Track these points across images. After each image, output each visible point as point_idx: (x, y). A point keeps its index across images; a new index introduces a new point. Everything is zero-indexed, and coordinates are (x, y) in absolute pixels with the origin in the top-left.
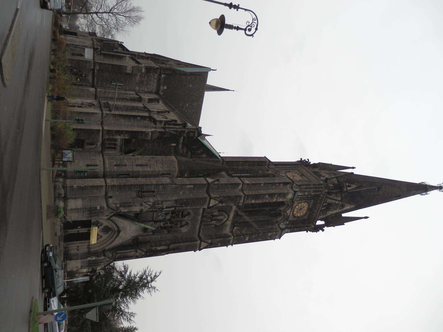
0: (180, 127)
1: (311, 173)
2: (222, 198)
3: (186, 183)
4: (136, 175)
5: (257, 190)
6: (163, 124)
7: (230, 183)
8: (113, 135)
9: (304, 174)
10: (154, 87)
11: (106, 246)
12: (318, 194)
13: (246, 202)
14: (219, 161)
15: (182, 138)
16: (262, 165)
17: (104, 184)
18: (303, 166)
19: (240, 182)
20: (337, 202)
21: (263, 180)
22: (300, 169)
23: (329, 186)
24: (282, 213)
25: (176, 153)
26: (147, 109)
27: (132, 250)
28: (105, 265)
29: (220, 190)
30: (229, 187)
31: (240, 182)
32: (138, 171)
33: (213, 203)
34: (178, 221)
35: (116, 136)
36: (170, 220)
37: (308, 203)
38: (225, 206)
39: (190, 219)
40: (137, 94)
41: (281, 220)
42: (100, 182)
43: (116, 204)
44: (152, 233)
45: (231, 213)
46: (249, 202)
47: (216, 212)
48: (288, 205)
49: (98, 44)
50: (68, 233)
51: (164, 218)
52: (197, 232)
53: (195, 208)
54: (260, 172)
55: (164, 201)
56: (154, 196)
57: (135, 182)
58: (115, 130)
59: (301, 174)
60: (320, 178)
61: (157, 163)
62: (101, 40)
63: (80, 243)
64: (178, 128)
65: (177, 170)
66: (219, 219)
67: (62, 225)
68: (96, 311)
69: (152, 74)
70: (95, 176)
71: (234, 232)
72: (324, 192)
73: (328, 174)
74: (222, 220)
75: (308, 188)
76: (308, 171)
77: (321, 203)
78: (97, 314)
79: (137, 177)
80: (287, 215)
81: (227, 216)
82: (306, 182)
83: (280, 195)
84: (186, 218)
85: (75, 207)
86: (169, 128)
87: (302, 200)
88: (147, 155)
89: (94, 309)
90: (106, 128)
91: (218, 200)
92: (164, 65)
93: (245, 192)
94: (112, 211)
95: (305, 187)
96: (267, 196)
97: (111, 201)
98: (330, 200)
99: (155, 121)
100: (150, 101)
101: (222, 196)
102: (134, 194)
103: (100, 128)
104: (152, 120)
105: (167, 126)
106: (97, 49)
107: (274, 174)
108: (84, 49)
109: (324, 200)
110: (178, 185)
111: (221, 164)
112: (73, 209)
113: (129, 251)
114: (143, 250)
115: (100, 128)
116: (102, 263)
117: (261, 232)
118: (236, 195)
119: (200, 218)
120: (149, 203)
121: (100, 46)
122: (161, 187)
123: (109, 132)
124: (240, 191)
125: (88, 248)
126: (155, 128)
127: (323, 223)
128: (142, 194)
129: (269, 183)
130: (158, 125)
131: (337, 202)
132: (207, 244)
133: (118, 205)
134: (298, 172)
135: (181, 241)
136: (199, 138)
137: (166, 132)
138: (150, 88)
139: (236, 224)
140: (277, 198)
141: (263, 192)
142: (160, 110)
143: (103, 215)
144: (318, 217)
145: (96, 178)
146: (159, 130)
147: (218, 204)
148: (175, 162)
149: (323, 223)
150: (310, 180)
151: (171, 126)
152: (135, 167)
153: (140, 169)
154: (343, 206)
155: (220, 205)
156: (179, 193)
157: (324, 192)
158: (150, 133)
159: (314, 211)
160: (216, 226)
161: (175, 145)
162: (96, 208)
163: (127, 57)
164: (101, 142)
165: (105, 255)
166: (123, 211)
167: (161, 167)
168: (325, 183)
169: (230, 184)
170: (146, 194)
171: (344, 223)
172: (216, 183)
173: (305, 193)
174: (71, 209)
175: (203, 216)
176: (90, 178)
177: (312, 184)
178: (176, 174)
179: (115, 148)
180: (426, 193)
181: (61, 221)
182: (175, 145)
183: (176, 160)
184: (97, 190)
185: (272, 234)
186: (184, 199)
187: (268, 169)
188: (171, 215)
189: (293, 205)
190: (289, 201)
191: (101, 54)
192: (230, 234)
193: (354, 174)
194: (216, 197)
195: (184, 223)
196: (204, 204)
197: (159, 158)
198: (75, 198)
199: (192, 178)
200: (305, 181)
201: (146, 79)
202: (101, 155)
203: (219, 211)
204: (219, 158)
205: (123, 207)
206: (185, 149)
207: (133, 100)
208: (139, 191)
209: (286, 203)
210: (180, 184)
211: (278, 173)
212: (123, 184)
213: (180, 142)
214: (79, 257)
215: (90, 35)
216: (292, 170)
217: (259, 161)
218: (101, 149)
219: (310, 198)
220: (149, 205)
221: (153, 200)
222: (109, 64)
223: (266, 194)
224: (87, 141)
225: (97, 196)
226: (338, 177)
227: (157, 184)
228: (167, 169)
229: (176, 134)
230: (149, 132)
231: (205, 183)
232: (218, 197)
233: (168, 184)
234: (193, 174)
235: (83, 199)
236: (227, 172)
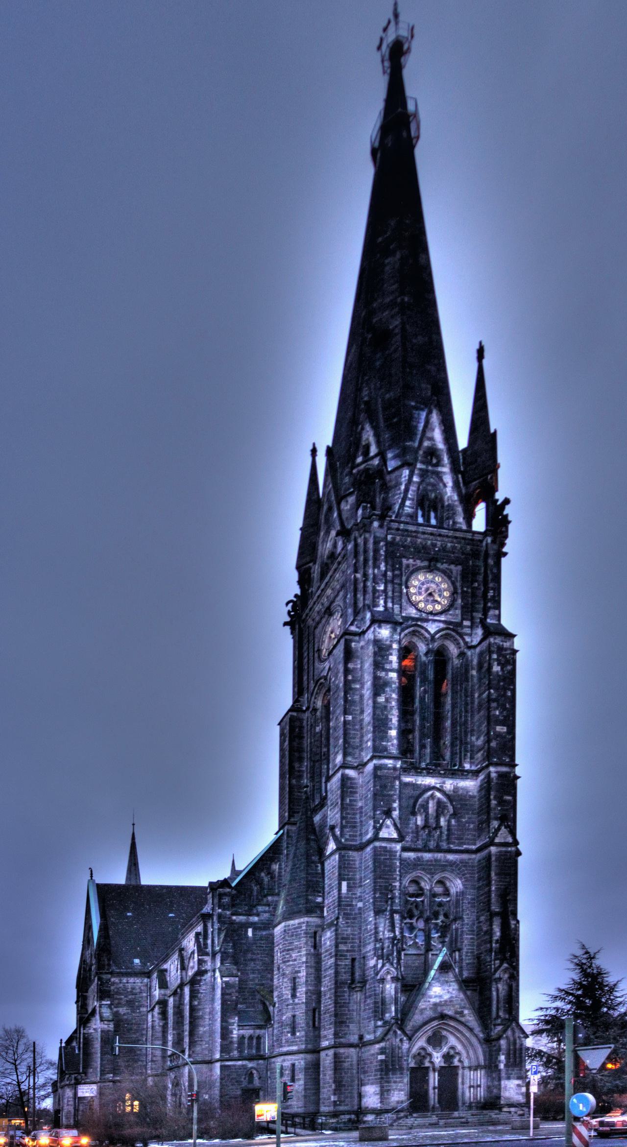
0: (209, 925)
1: (322, 586)
2: (378, 812)
3: (337, 897)
4: (316, 995)
5: (362, 728)
6: (206, 958)
7: (339, 801)
8: (232, 1042)
9: (326, 604)
10: (138, 981)
11: (476, 1036)
12: (384, 549)
13: (394, 751)
14: (288, 832)
15: (234, 918)
16: (301, 728)
17: (331, 1052)
18: (304, 616)
19: (339, 775)
20: (416, 479)
21: (337, 718)
22: (313, 620)
23: (363, 518)
24: (436, 645)
25: (269, 925)
26: (179, 990)
27: (493, 989)
28: (522, 1036)
29: (358, 820)
30: (350, 800)
31: (339, 775)
32: (306, 993)
33: (389, 832)
34: (432, 903)
35: (232, 1038)
36: (427, 921)
37: (412, 573)
38: (400, 801)
39: (429, 876)
40: (152, 1010)
41: (458, 644)
42: (327, 1059)
43: (376, 1027)
44: (457, 953)
45: (423, 783)
46: (392, 745)
47: (416, 819)
48: (414, 633)
49: (68, 1078)
50: (437, 1105)
51: (421, 933)
52: (465, 856)
53: (400, 871)
54: (318, 729)
55: (375, 937)
56: (364, 958)
57: (330, 998)
58: (219, 1040)
59: (327, 616)
60: (340, 554)
61: (289, 961)
62: (62, 1073)
63: (463, 1084)
64: (212, 928)
65: (306, 919)
66: (437, 811)
67: (415, 1115)
68: (588, 1051)
69: (112, 988)
70: (314, 1069)
71: (479, 766)
72: (380, 533)
73: (328, 533)
74: (439, 803)
75: (365, 587)
76: (319, 597)
77: (415, 532)
78: (593, 1049)
79: (319, 994)
80: (442, 630)
81: (430, 793)
82: (349, 596)
83: (379, 664)
84: (426, 886)
85: (378, 1097)
86: (213, 946)
87: (401, 592)
88: (272, 980)
89: (582, 1054)
90: (218, 1056)
91: (381, 821)
92: (93, 968)
93: (365, 760)
94: (391, 1033)
95: (360, 596)
96: (381, 699)
97: (368, 1037)
98: (408, 503)
99: (201, 973)
100: (163, 984)
101: (372, 814)
102: (358, 996)
103: (218, 1065)
104: (199, 978)
105: (209, 949)
106: (76, 1079)
107: (324, 691)
108: (80, 1098)
109: (407, 523)
110: (339, 913)
111: (294, 828)
112: (381, 1098)
113: (494, 993)
114: (497, 966)
115: (218, 1065)
116: (518, 1041)
117: (485, 695)
118: (372, 781)
119: (427, 856)
120: (379, 966)
121: (70, 1074)
122: (342, 947)
123: (225, 1049)
124: (362, 773)
125: (476, 1069)
126: (214, 971)
127: (481, 510)
128: (356, 981)
129: (346, 700)
130: (208, 966)
131: (416, 479)
132: (503, 828)
133: (380, 1023)
134: (320, 626)
135: (486, 889)
136: (233, 885)
137: (223, 950)
138: (140, 988)
139: (455, 765)
140: (387, 671)
141: (368, 711)
142: (179, 966)
143: (400, 1048)
144: (460, 530)
145: (319, 1064)
146: (218, 964)
147: (394, 820)
148: (289, 926)
149: (481, 510)
150: (343, 586)
151: (209, 942)
152: (296, 1001)
153: (302, 990)
154: (432, 452)
155: (396, 814)
156: (360, 909)
157: (380, 533)
158: (225, 979)
159: (439, 550)
160: (454, 815)
161: (250, 933)
162: (381, 1061)
163: (85, 1031)
164: (245, 1062)
165: (499, 1038)
166: (393, 1014)
167: (299, 952)
168: (352, 537)
169: (343, 799)
170: (357, 974)
171: (492, 431)
172: (338, 832)
173: (378, 591)
174: (381, 1102)
175: (426, 850)
176: (319, 1075)
177: (355, 576)
178: (314, 920)
179: (259, 1038)
180: (411, 118)
181: (406, 1117)
182: (250, 933)
183: (283, 924)
184: (345, 1062)
185: (496, 663)
186: (374, 898)
187: (311, 709)
188: (416, 918)
189: (413, 619)
190: (400, 635)
191: (85, 1073)
192: (482, 777)
193: (330, 444)
194: (374, 827)
195: (439, 889)
196: (392, 853)
197: (278, 956)
198: (360, 1096)
199: (326, 886)
200: (345, 597)
201: (123, 997)
202: (273, 1060)
203: (414, 813)
204: (283, 834)
205: (383, 1014)
206: (260, 908)
207: (164, 1014)
208: (349, 987)
209: (404, 642)
210: (338, 910)
211: (322, 680)
212: (333, 1019)
213: (243, 921)
214: (496, 1083)
215: (57, 1090)
216: (314, 645)
217: (290, 737)
218: (261, 1062)
219: (397, 572)
220: (383, 966)
221: (373, 958)
222: (102, 1060)
223: (375, 702)
224: (245, 1084)
225: (358, 1061)
226: (337, 496)
227: (336, 955)
228: (304, 940)
229: (224, 932)
230: (223, 982)
231: (337, 856)
232: (375, 822)
233: (336, 934)
234: (315, 885)
235: (362, 1084)
236: (316, 810)
